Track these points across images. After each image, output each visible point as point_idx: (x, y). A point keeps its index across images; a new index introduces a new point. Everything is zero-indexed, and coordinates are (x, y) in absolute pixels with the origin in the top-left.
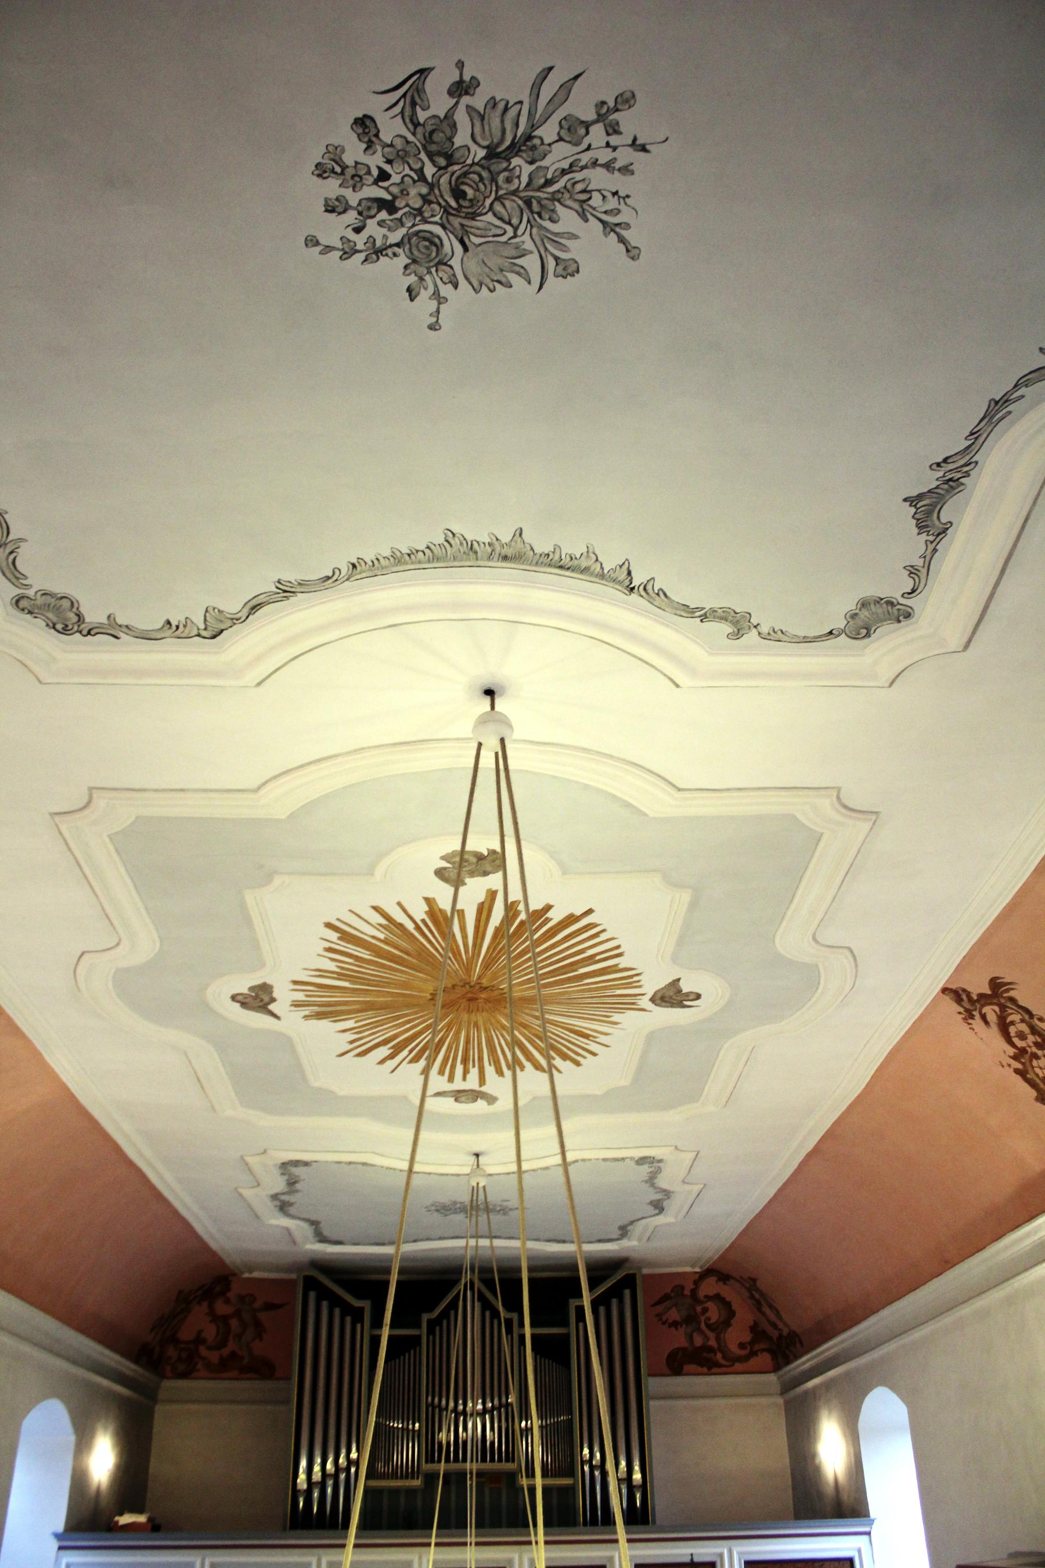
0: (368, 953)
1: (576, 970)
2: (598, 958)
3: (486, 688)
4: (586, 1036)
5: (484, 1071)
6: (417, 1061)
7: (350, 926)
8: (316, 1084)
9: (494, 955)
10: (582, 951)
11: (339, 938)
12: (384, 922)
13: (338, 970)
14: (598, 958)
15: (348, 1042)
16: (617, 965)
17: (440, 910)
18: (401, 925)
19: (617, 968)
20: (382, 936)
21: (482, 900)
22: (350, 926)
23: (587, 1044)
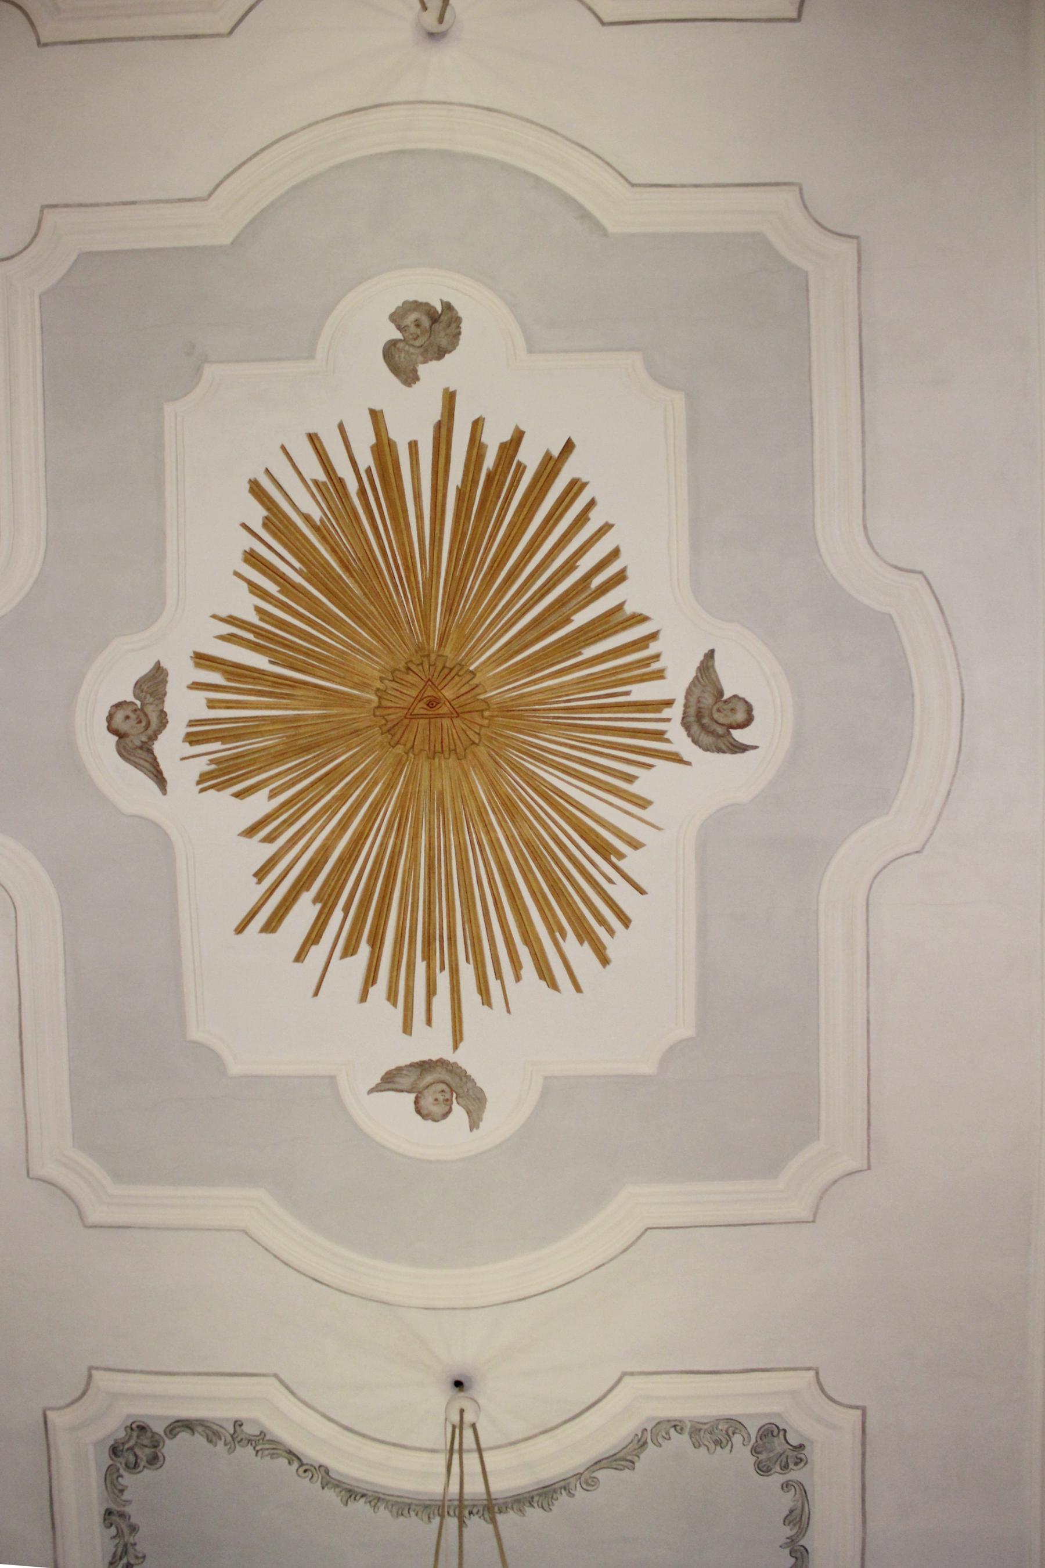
0: (297, 565)
1: (567, 621)
2: (597, 581)
3: (459, 1379)
4: (605, 850)
5: (457, 970)
6: (354, 952)
7: (280, 487)
8: (195, 1034)
9: (458, 573)
10: (569, 566)
11: (279, 592)
12: (322, 477)
13: (254, 618)
14: (597, 581)
15: (241, 834)
16: (620, 607)
17: (389, 440)
18: (341, 480)
19: (618, 617)
20: (316, 515)
21: (439, 418)
22: (280, 487)
23: (610, 881)
